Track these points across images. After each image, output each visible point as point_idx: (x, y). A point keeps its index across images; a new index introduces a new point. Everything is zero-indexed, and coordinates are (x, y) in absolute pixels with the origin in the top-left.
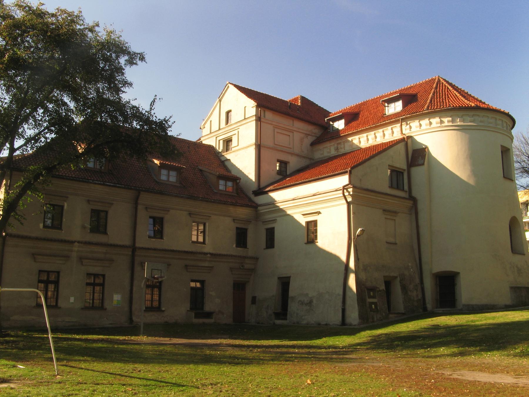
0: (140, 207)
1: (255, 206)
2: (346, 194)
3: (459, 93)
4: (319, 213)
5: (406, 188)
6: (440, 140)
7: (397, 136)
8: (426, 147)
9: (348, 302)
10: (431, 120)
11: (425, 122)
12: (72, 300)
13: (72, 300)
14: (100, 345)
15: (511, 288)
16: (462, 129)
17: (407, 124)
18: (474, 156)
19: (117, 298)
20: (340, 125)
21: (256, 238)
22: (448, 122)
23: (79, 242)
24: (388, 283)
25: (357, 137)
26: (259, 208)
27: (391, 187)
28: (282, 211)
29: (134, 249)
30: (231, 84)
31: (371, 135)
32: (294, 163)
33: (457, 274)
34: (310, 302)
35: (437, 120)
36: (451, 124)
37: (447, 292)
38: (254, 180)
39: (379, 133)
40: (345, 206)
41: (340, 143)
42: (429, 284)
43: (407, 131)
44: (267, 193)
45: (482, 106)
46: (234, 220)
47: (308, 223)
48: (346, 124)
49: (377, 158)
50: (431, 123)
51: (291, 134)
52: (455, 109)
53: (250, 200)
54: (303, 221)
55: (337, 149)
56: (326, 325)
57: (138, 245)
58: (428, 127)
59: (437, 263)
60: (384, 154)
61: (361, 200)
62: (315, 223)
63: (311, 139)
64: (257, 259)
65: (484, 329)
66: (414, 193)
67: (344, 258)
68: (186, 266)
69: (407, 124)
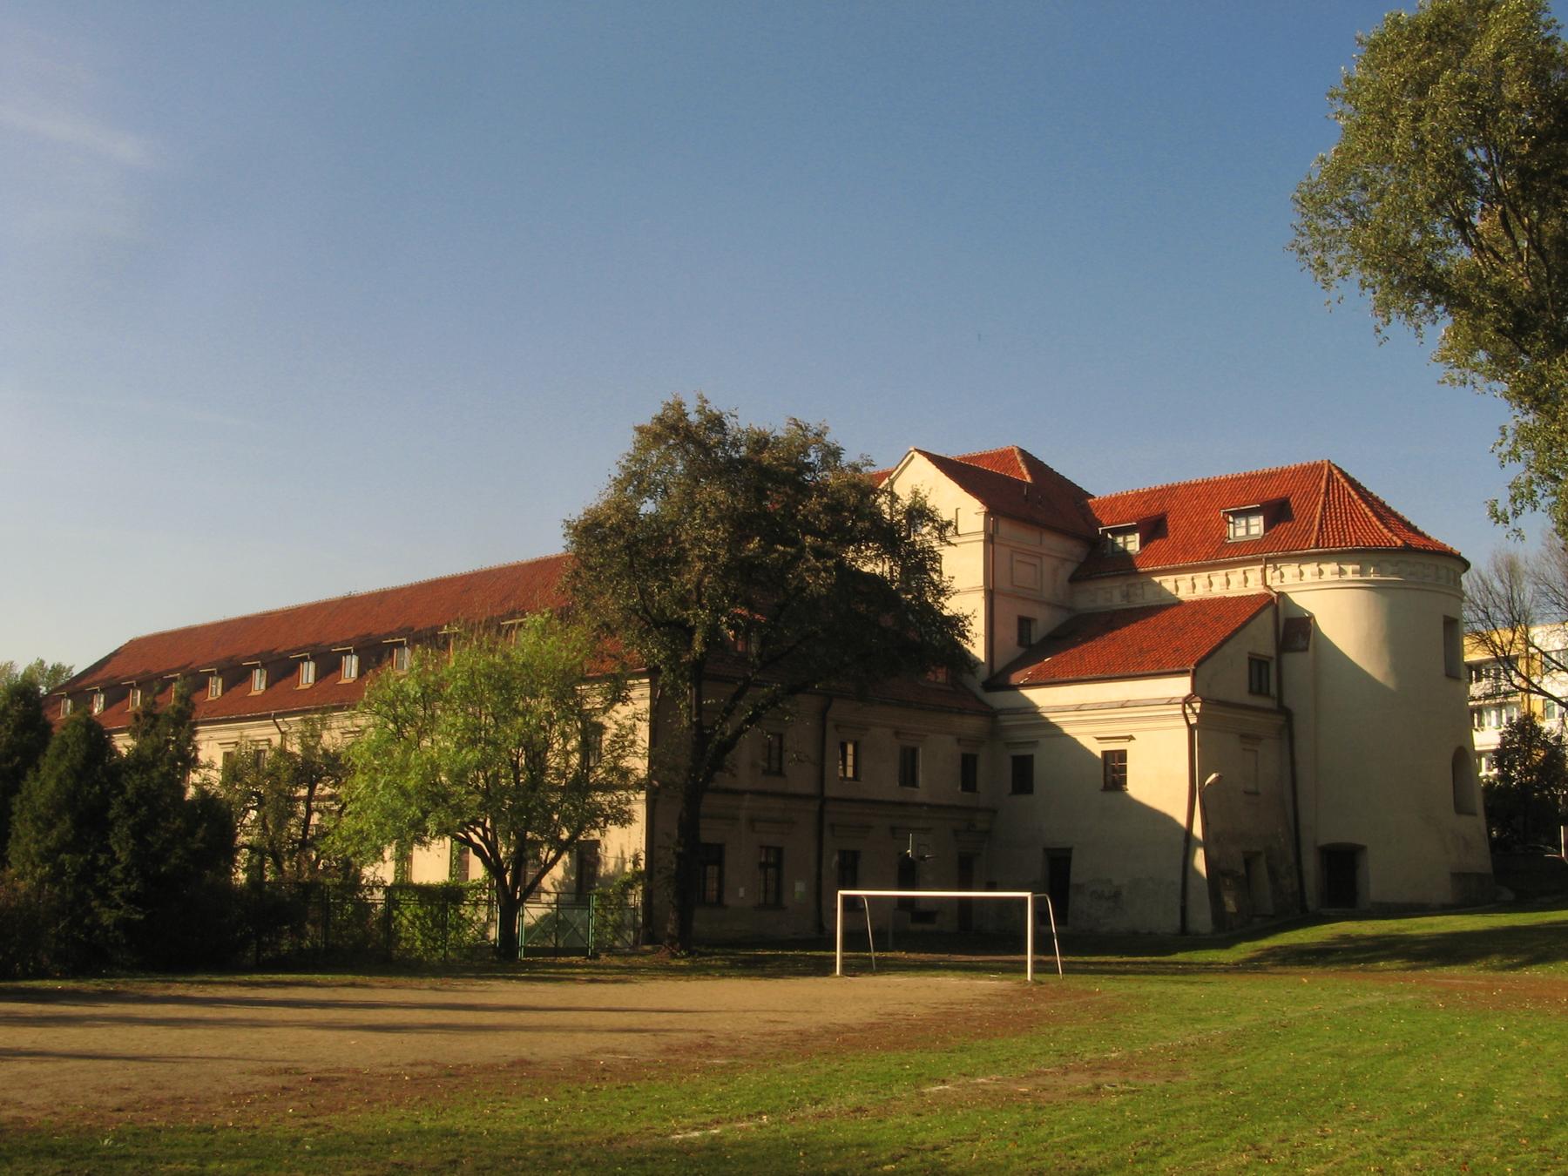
0: (830, 725)
1: (992, 714)
2: (1189, 711)
3: (1358, 493)
4: (1131, 738)
5: (1273, 690)
6: (1335, 604)
7: (1254, 587)
8: (1311, 616)
9: (1192, 896)
10: (1323, 567)
11: (1310, 569)
12: (742, 892)
13: (742, 892)
14: (59, 985)
15: (1454, 875)
16: (1377, 587)
17: (1276, 569)
18: (1397, 637)
19: (800, 887)
20: (1133, 543)
21: (994, 774)
22: (1354, 572)
23: (751, 792)
24: (1248, 862)
25: (1171, 578)
26: (1001, 717)
27: (1251, 691)
28: (1053, 726)
29: (822, 799)
30: (920, 452)
31: (1201, 578)
32: (1045, 621)
33: (1362, 848)
34: (1116, 895)
35: (1334, 567)
36: (1358, 577)
37: (1341, 881)
38: (982, 658)
39: (1218, 577)
40: (1185, 732)
41: (1133, 585)
42: (1311, 864)
43: (1275, 583)
44: (1016, 688)
45: (1415, 542)
46: (959, 740)
47: (1105, 753)
48: (1143, 544)
49: (1232, 642)
50: (1321, 572)
51: (1037, 561)
52: (1366, 551)
53: (981, 702)
54: (1097, 749)
55: (1126, 596)
56: (1150, 933)
57: (830, 792)
58: (1316, 579)
59: (1327, 828)
60: (1241, 633)
61: (1214, 727)
62: (1122, 755)
63: (1070, 568)
64: (994, 812)
65: (1425, 942)
66: (1287, 702)
67: (1182, 820)
68: (893, 829)
69: (1276, 569)
